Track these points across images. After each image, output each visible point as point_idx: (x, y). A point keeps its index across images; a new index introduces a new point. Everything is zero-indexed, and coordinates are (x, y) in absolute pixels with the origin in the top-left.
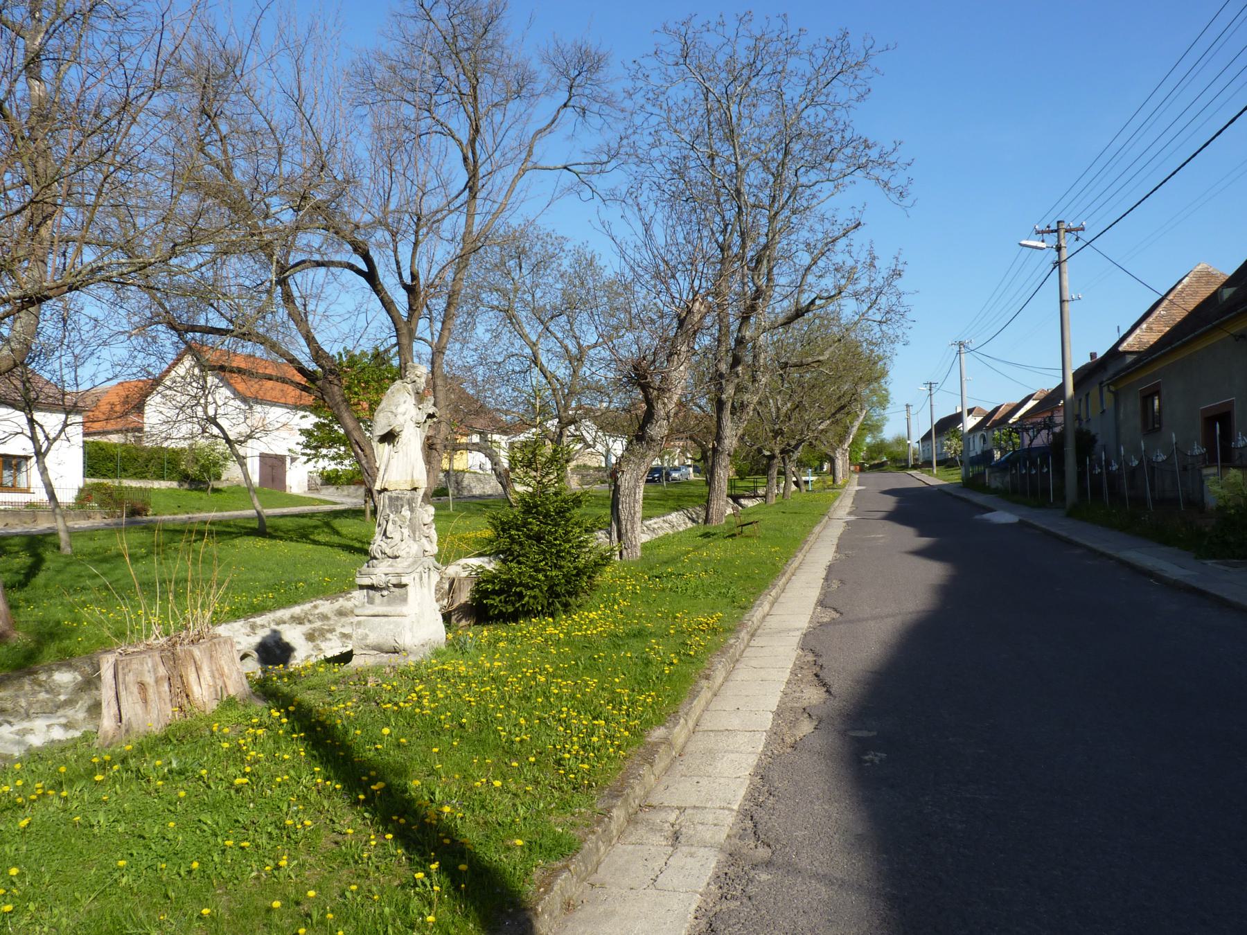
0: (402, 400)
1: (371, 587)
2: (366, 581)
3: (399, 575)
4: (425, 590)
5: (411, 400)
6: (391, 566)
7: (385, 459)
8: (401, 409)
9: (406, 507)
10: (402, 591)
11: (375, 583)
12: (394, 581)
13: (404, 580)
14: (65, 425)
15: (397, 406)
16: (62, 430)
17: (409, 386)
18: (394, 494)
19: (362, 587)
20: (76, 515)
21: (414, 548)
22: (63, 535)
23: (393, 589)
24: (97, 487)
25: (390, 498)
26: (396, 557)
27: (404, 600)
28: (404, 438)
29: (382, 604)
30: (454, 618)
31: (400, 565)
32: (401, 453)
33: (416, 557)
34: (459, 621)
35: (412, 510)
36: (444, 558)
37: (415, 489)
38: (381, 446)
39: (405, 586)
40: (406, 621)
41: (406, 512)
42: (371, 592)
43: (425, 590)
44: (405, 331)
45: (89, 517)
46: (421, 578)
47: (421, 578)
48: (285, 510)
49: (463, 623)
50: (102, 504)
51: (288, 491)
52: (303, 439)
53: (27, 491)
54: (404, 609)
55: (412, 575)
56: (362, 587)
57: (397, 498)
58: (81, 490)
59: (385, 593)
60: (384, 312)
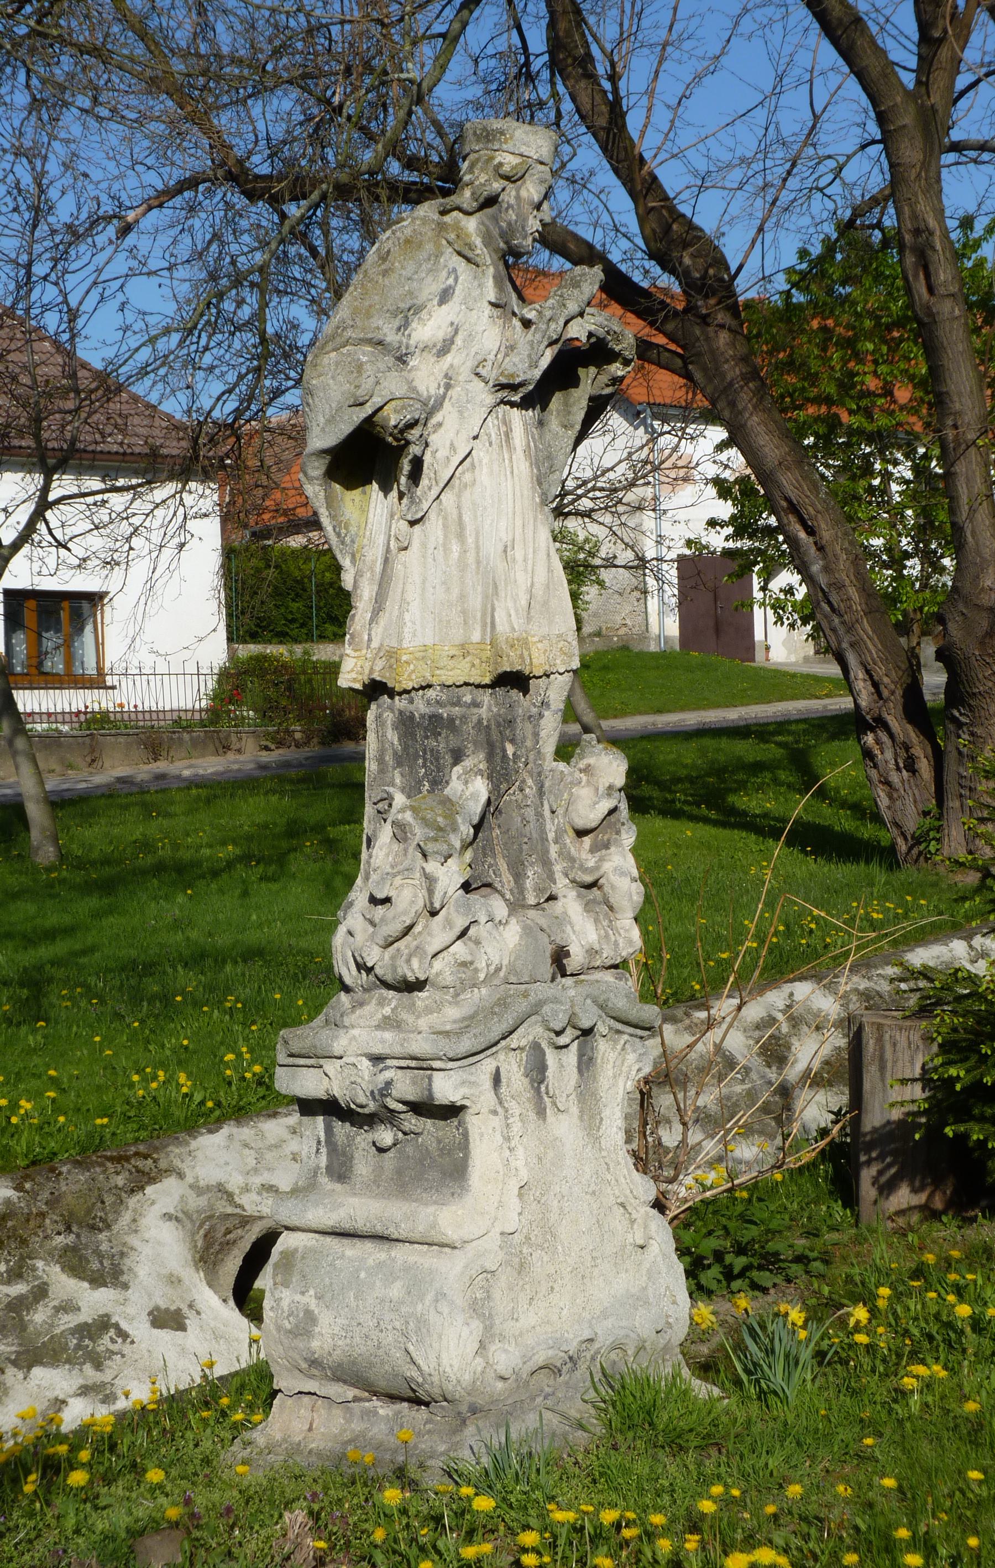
0: (431, 288)
1: (328, 1107)
2: (309, 1084)
3: (421, 1065)
4: (565, 1126)
5: (479, 287)
6: (388, 1023)
7: (374, 554)
8: (427, 330)
9: (475, 760)
10: (448, 1129)
11: (338, 1092)
12: (405, 1087)
13: (446, 1088)
14: (43, 505)
15: (407, 314)
16: (39, 514)
17: (471, 224)
18: (420, 706)
19: (309, 1107)
20: (195, 743)
21: (503, 940)
22: (35, 812)
23: (411, 1122)
24: (259, 666)
25: (406, 723)
26: (412, 986)
27: (453, 1170)
28: (443, 444)
29: (376, 1187)
30: (867, 1175)
31: (428, 1023)
32: (434, 525)
33: (510, 979)
34: (887, 1189)
35: (501, 775)
36: (677, 975)
37: (515, 681)
38: (351, 500)
39: (452, 1111)
40: (451, 1270)
41: (470, 788)
42: (342, 1129)
43: (565, 1126)
44: (907, 118)
45: (227, 748)
46: (537, 1072)
47: (537, 1072)
48: (712, 716)
49: (903, 1197)
50: (267, 711)
51: (759, 655)
52: (725, 510)
53: (97, 682)
54: (448, 1218)
55: (487, 1066)
56: (309, 1107)
57: (435, 723)
58: (224, 675)
59: (386, 1136)
60: (828, 54)
